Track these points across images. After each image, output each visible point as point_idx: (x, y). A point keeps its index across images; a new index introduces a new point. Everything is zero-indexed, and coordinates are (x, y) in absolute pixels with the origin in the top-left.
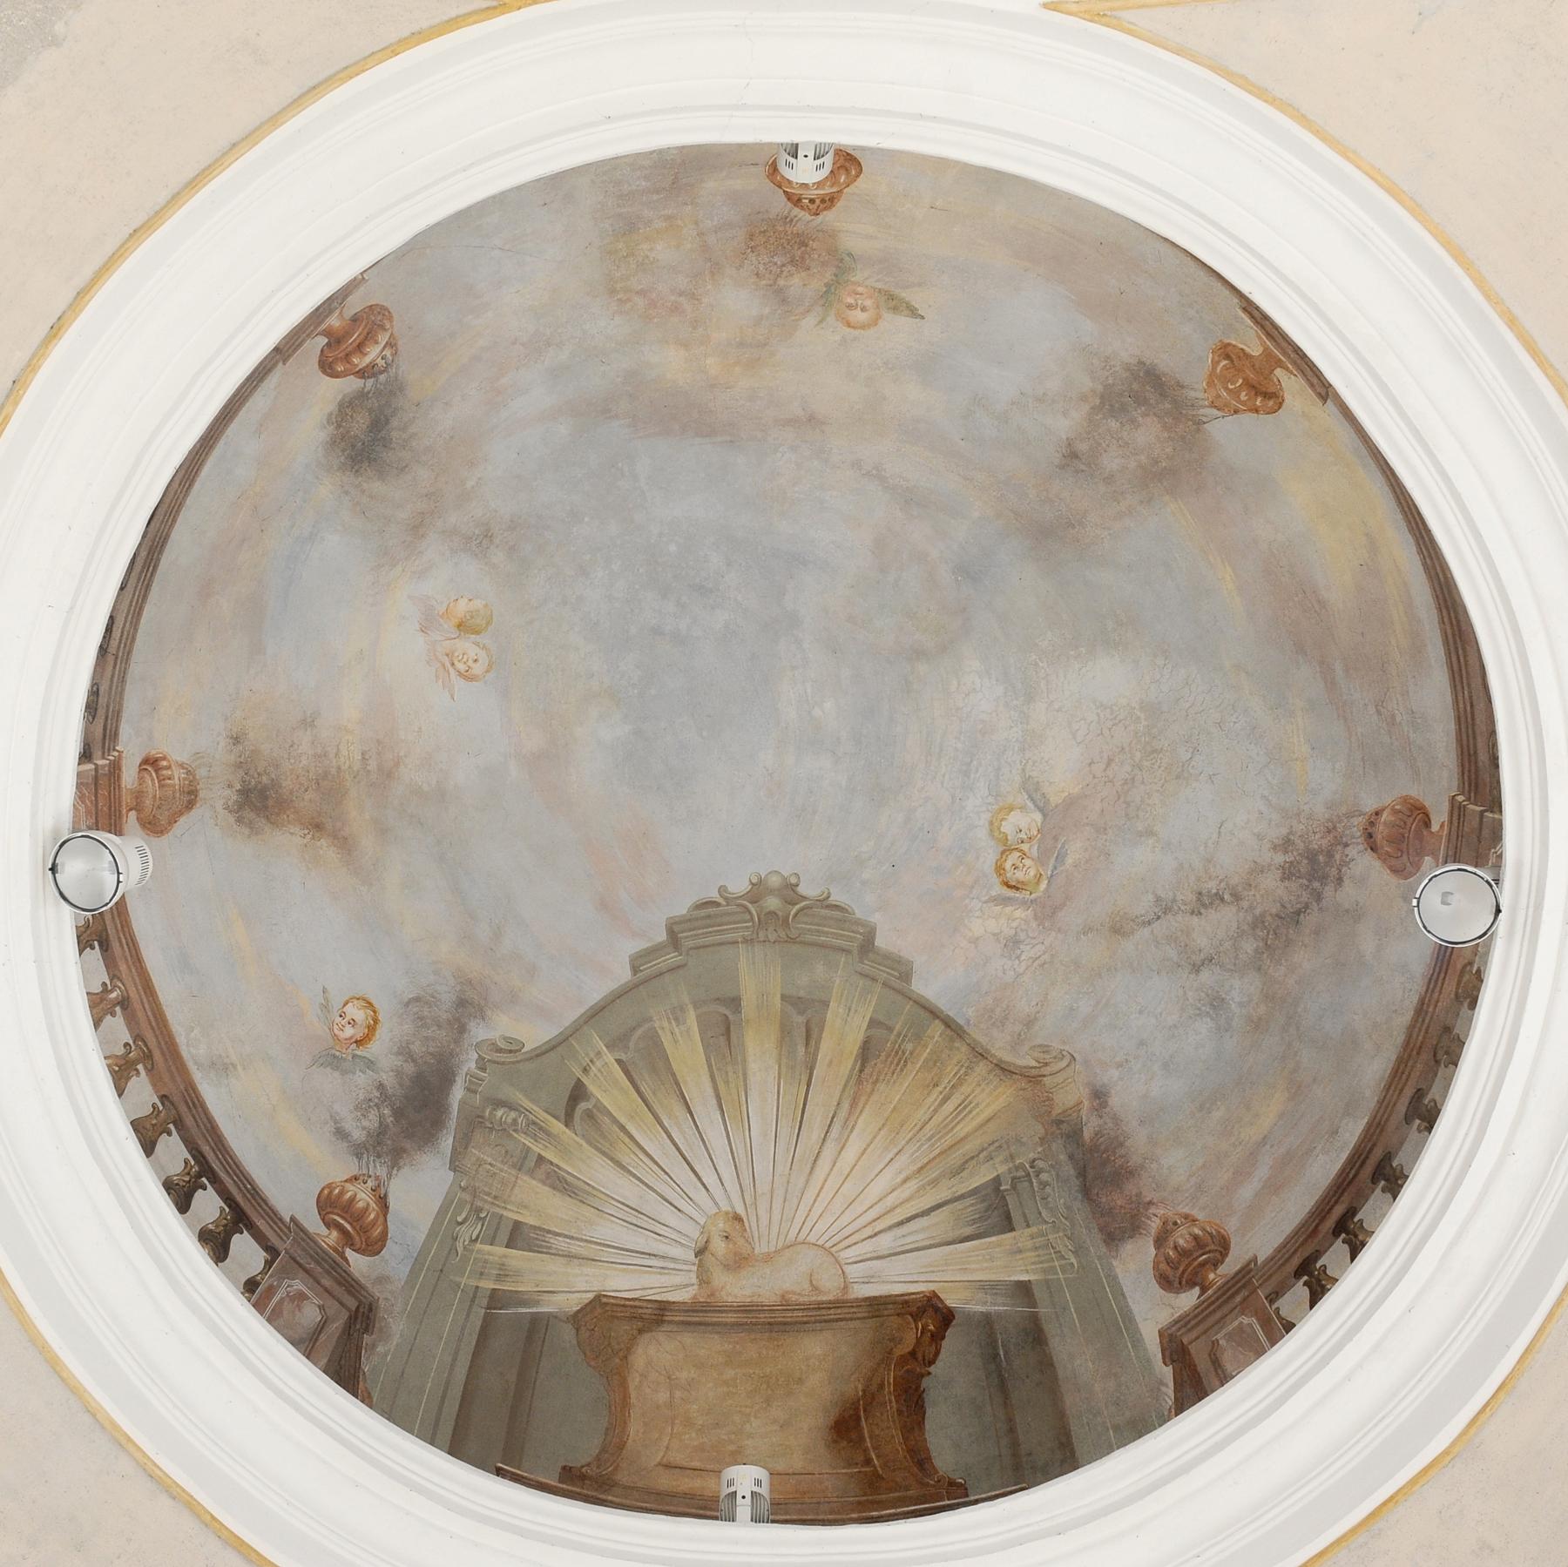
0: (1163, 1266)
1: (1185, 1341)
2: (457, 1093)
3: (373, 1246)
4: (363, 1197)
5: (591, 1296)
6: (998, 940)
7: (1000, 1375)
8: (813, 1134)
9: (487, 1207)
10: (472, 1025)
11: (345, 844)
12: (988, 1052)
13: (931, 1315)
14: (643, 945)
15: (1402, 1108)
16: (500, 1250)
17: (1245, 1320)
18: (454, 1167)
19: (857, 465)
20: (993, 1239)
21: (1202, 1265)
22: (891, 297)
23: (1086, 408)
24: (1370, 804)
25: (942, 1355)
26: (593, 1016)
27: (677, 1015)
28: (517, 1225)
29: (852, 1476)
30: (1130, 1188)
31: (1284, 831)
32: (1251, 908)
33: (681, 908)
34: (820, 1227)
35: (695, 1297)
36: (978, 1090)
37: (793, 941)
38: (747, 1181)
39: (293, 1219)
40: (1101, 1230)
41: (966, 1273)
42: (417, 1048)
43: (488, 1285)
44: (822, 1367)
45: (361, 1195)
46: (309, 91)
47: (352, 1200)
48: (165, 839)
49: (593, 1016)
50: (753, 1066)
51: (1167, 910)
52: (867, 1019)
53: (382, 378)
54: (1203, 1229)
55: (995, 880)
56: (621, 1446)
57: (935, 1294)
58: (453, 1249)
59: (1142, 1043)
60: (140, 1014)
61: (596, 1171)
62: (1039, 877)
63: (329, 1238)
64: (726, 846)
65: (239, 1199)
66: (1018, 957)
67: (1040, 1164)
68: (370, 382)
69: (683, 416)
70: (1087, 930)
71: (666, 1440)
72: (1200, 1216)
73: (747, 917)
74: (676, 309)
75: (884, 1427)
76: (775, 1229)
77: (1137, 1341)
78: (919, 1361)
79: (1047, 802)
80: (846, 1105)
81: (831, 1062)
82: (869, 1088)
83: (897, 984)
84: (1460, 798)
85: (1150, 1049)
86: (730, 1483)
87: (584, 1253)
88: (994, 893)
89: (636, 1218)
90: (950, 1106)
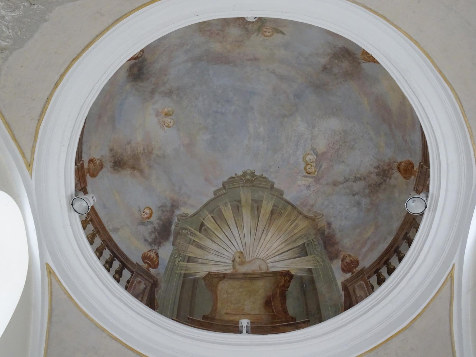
0: (343, 267)
2: (173, 227)
3: (155, 266)
4: (152, 255)
5: (208, 273)
11: (141, 171)
13: (288, 275)
14: (216, 188)
15: (402, 236)
16: (186, 263)
17: (362, 282)
18: (173, 245)
19: (268, 70)
21: (353, 267)
22: (276, 29)
23: (329, 57)
24: (399, 160)
27: (226, 205)
28: (189, 257)
31: (377, 164)
33: (226, 179)
37: (254, 186)
38: (244, 244)
41: (296, 266)
42: (162, 218)
43: (183, 272)
44: (262, 288)
46: (115, 21)
47: (150, 256)
48: (96, 178)
50: (245, 219)
51: (347, 181)
53: (140, 59)
55: (304, 171)
56: (216, 309)
57: (289, 271)
58: (174, 265)
60: (96, 222)
61: (207, 243)
62: (315, 171)
64: (237, 163)
67: (314, 240)
68: (137, 61)
69: (221, 60)
70: (327, 184)
71: (226, 308)
72: (352, 255)
74: (218, 34)
75: (277, 303)
76: (251, 256)
77: (336, 285)
78: (286, 286)
79: (318, 153)
80: (267, 226)
83: (280, 196)
84: (422, 163)
85: (341, 213)
86: (241, 323)
89: (218, 254)
90: (292, 226)
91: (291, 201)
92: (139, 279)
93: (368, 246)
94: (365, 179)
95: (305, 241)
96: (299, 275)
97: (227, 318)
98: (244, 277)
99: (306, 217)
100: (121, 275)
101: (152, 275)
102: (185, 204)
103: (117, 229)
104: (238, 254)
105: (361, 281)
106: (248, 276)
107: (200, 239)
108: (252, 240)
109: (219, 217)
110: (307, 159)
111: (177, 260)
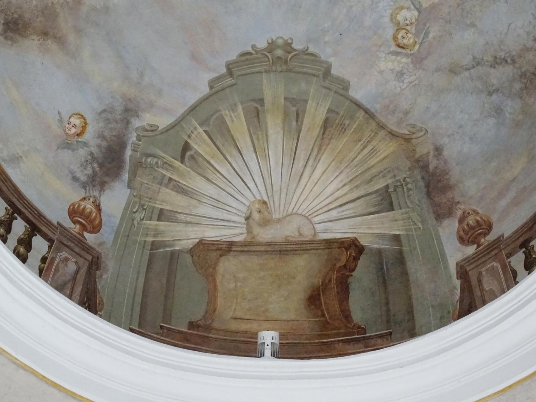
0: (462, 233)
1: (468, 270)
2: (128, 153)
3: (96, 229)
4: (89, 207)
5: (197, 240)
6: (393, 72)
7: (384, 278)
8: (300, 164)
9: (147, 203)
10: (133, 120)
11: (61, 41)
12: (385, 125)
13: (353, 248)
14: (214, 75)
16: (154, 222)
17: (495, 264)
18: (130, 186)
20: (384, 214)
21: (480, 234)
25: (357, 268)
26: (192, 110)
28: (161, 210)
29: (316, 322)
30: (449, 195)
32: (520, 68)
33: (233, 56)
34: (303, 207)
35: (245, 239)
36: (380, 144)
37: (289, 71)
38: (269, 186)
39: (58, 223)
40: (434, 212)
41: (371, 229)
42: (107, 134)
43: (150, 239)
44: (304, 271)
45: (88, 206)
47: (84, 209)
49: (192, 110)
50: (271, 131)
51: (478, 64)
52: (327, 108)
54: (481, 218)
55: (393, 43)
56: (214, 310)
57: (356, 239)
59: (461, 127)
61: (198, 183)
63: (75, 229)
65: (33, 219)
66: (403, 81)
67: (408, 180)
70: (437, 70)
71: (234, 305)
72: (480, 211)
73: (266, 59)
75: (330, 300)
76: (282, 208)
77: (446, 267)
78: (349, 268)
79: (421, 6)
80: (316, 150)
81: (309, 129)
82: (327, 142)
83: (342, 92)
86: (262, 338)
87: (193, 220)
88: (392, 50)
89: (217, 203)
90: (366, 151)
91: (364, 102)
92: (64, 254)
93: (512, 194)
94: (514, 61)
95: (390, 181)
96: (376, 246)
97: (234, 326)
98: (269, 248)
99: (393, 135)
100: (29, 247)
101: (91, 247)
102: (152, 105)
103: (17, 159)
104: (257, 206)
105: (494, 260)
106: (276, 248)
107: (182, 175)
108: (286, 179)
109: (220, 134)
110: (400, 18)
111: (138, 216)
